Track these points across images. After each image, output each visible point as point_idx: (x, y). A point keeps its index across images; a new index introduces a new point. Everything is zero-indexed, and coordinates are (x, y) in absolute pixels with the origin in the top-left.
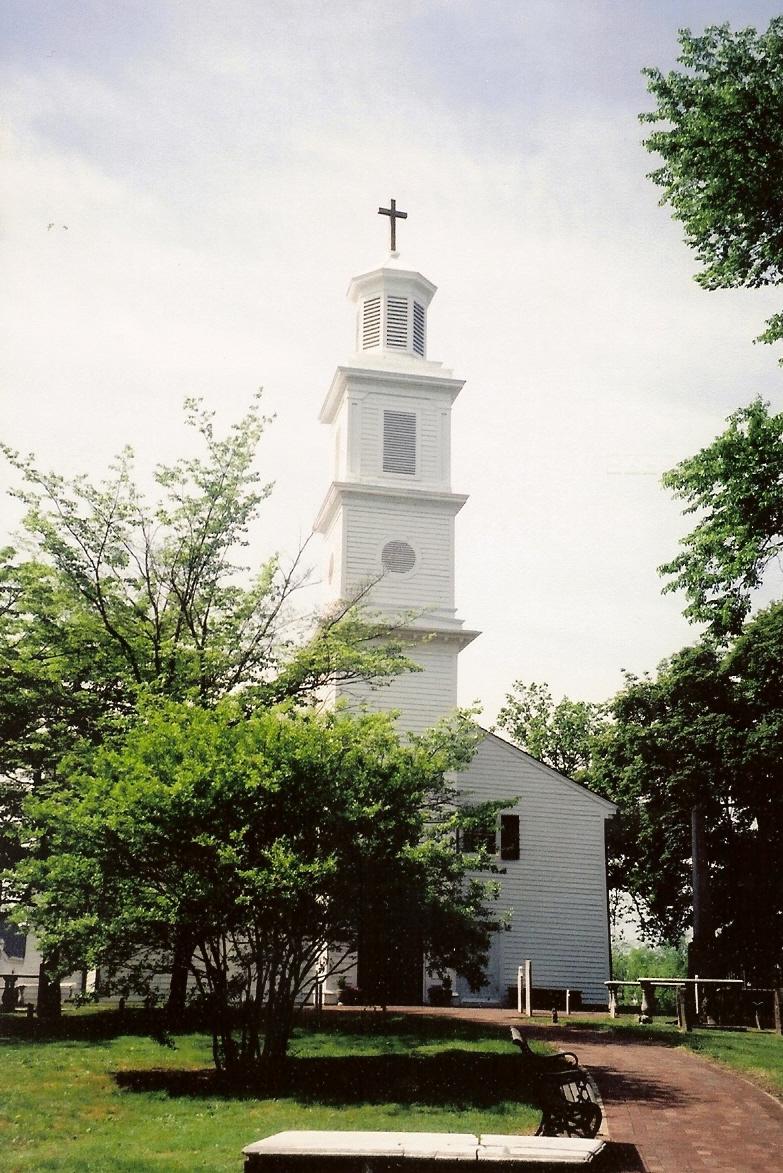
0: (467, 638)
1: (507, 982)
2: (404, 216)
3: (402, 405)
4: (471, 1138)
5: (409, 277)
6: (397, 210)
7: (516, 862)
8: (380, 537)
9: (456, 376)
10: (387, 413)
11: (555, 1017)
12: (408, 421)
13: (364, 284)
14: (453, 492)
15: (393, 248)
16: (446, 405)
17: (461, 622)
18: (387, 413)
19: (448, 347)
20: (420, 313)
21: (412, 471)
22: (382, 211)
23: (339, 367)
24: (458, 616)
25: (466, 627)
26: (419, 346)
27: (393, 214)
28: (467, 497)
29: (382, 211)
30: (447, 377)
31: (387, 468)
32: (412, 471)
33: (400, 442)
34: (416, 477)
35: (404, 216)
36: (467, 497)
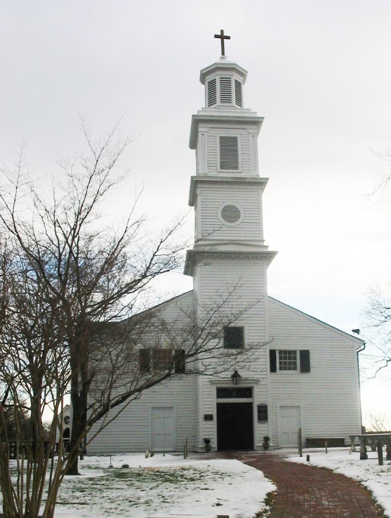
0: (270, 255)
1: (305, 436)
2: (228, 38)
3: (230, 133)
4: (383, 452)
5: (193, 185)
6: (220, 39)
7: (264, 423)
8: (220, 204)
9: (258, 115)
10: (221, 138)
11: (308, 459)
12: (234, 140)
13: (193, 116)
14: (261, 177)
15: (223, 53)
16: (256, 131)
17: (267, 247)
18: (221, 138)
19: (253, 101)
20: (238, 85)
21: (237, 168)
22: (216, 36)
23: (193, 115)
24: (265, 244)
25: (270, 249)
26: (239, 101)
27: (222, 37)
28: (268, 179)
29: (216, 36)
30: (254, 116)
31: (222, 167)
32: (237, 168)
33: (229, 151)
34: (239, 170)
35: (228, 38)
36: (268, 179)
